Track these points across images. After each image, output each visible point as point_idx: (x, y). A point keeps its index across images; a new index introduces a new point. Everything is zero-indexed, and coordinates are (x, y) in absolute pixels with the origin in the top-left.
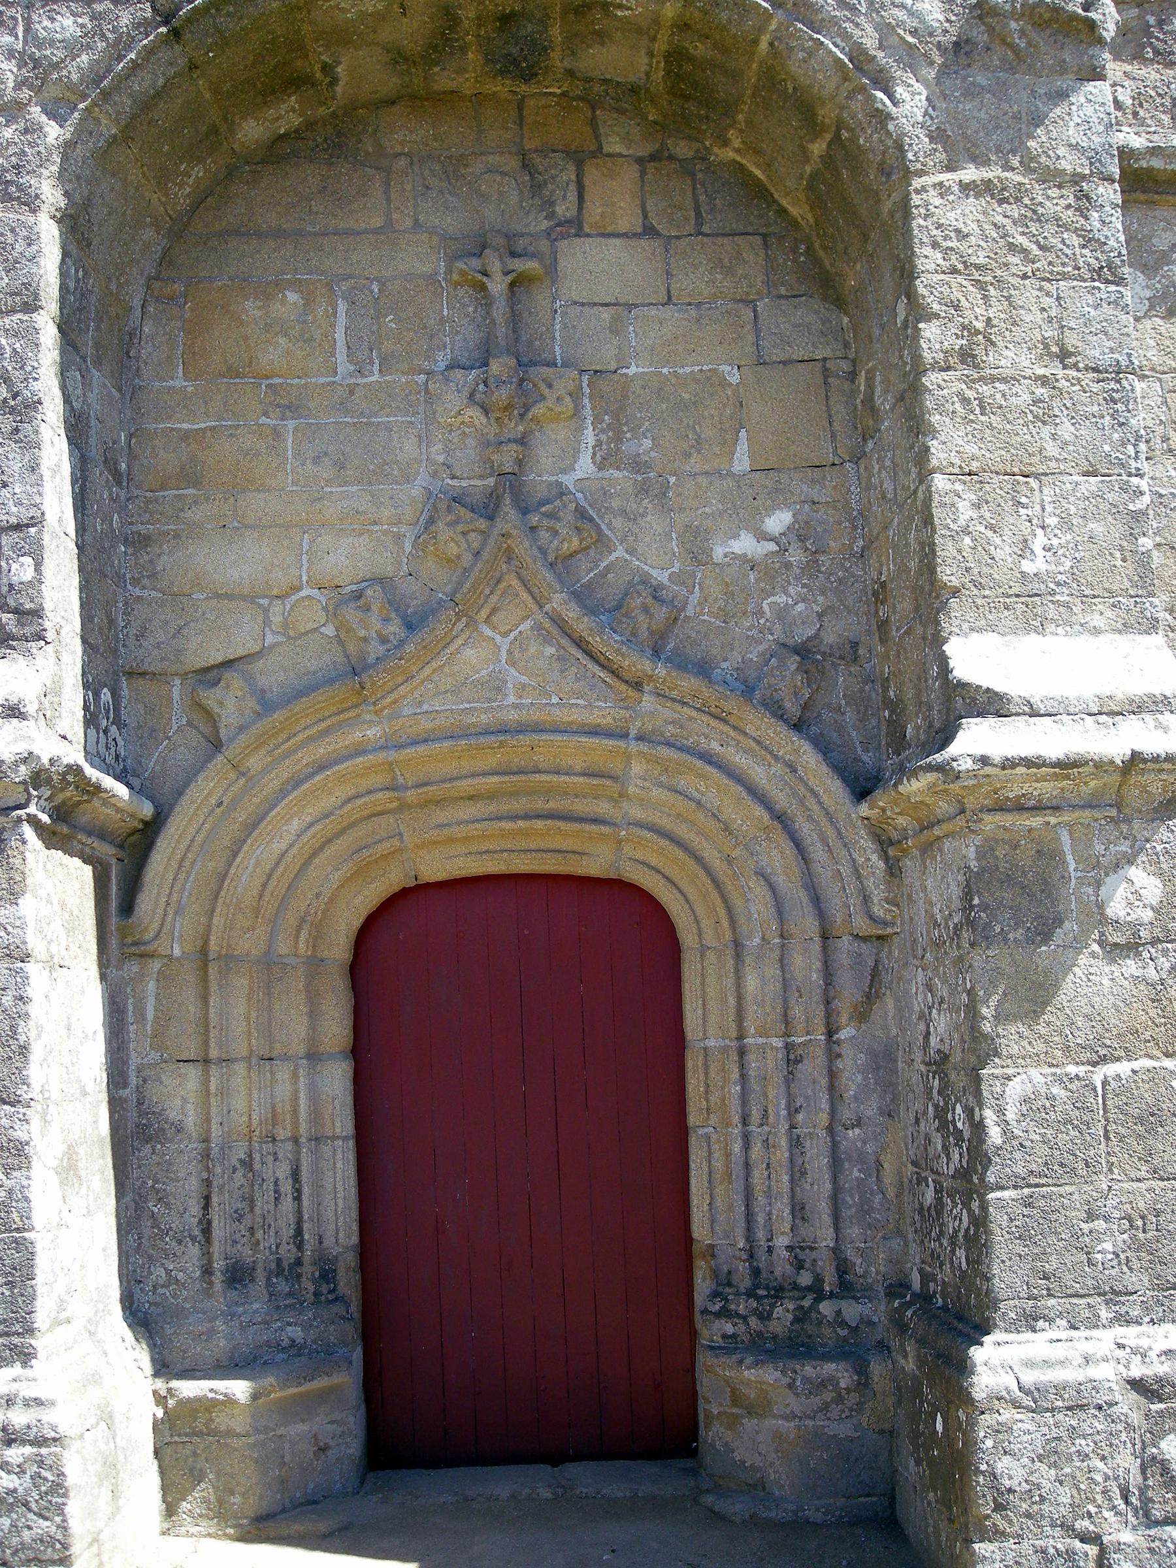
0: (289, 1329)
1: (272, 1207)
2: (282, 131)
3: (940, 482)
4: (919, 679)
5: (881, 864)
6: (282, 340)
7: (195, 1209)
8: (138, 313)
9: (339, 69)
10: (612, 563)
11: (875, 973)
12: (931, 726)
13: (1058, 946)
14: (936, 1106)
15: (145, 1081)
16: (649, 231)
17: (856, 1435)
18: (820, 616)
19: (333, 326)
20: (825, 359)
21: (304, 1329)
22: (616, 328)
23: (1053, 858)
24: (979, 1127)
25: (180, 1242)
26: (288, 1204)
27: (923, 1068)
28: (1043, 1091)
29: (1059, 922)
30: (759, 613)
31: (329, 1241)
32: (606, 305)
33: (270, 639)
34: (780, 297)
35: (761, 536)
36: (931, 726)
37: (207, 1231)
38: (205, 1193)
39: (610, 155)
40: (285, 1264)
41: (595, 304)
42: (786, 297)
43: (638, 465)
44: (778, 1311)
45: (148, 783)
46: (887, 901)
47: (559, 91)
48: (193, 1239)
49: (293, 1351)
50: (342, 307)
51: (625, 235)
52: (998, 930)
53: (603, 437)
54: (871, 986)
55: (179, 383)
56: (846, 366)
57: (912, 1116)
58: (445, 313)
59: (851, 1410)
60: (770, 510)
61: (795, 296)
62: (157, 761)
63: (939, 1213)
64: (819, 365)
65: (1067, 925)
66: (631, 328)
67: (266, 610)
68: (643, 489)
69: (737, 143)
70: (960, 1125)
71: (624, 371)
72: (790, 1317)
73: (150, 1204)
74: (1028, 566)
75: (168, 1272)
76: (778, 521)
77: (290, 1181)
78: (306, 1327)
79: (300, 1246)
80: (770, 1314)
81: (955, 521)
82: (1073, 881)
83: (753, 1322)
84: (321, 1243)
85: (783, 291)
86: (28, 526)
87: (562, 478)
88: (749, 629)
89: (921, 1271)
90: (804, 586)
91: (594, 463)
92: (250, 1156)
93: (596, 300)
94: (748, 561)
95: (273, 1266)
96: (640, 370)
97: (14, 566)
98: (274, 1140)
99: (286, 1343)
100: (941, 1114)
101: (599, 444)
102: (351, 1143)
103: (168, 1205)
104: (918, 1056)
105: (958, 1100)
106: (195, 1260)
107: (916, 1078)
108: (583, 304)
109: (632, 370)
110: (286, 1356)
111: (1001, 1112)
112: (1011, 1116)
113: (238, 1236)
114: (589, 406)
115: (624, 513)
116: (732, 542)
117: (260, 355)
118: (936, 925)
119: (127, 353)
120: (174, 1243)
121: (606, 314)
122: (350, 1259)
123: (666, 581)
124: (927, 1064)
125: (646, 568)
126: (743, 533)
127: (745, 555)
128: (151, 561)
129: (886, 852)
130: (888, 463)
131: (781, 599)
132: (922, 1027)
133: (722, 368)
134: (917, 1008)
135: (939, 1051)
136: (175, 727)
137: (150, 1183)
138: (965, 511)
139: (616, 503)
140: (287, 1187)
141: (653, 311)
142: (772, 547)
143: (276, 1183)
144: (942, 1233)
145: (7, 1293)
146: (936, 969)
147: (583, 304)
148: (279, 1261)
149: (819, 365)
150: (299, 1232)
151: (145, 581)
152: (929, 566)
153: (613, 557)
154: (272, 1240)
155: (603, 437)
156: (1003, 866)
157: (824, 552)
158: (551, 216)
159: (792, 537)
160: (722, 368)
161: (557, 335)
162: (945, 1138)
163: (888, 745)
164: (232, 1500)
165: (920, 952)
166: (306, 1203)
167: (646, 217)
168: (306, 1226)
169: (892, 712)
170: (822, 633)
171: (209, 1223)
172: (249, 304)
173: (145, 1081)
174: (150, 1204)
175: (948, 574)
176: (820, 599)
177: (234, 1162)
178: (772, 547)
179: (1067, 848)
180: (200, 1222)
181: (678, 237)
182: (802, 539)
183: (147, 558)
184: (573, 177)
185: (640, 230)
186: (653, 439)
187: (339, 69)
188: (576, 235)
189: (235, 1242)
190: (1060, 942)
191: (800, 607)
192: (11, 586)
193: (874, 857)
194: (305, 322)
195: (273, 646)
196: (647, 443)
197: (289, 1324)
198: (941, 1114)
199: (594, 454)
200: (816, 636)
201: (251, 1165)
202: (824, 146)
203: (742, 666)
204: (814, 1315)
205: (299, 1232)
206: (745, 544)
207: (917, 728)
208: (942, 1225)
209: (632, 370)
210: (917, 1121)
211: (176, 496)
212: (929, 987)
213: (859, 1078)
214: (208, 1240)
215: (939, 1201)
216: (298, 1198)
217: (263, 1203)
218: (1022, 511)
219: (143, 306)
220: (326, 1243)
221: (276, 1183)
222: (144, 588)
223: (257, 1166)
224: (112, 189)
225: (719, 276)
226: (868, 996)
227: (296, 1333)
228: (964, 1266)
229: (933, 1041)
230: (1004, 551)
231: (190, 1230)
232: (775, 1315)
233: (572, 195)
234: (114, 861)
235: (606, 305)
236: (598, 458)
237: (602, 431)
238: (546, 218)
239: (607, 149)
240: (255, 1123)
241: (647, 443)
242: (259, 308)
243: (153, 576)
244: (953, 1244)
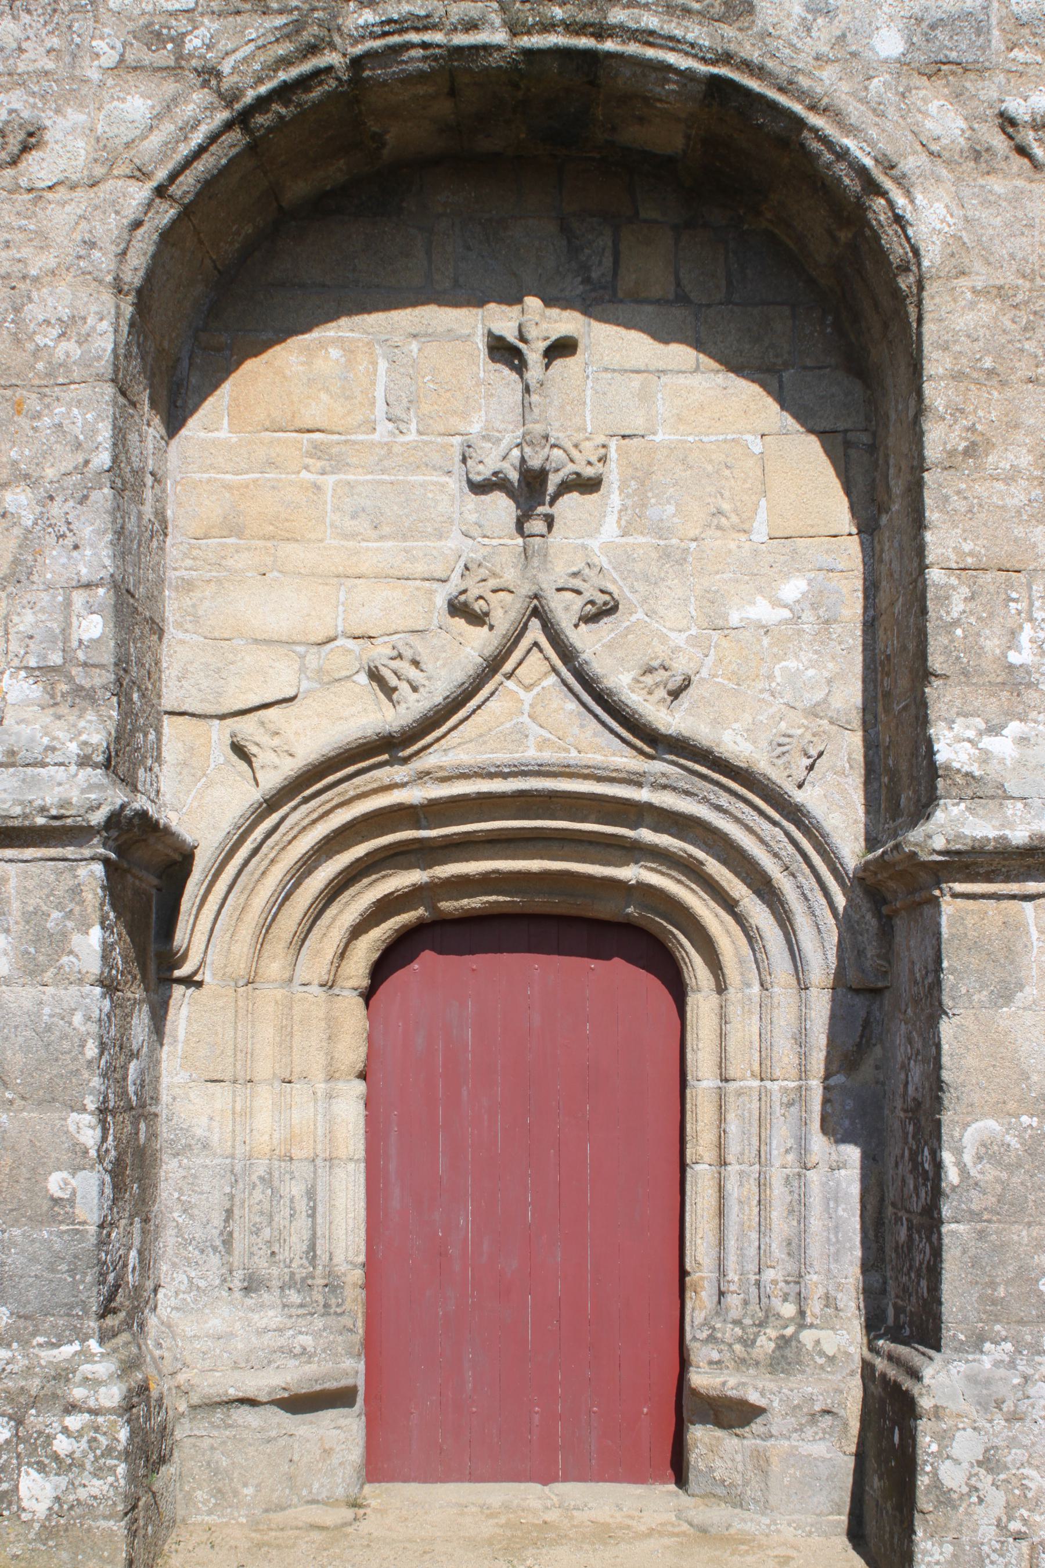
0: (301, 1337)
1: (287, 1223)
2: (328, 187)
3: (934, 575)
4: (912, 755)
5: (874, 922)
6: (324, 396)
7: (218, 1220)
8: (185, 363)
9: (387, 137)
10: (634, 624)
11: (866, 1024)
12: (919, 800)
13: (1019, 1008)
14: (910, 1149)
15: (174, 1099)
16: (682, 298)
17: (828, 1456)
18: (829, 682)
19: (373, 383)
20: (846, 431)
21: (315, 1338)
22: (645, 396)
23: (1017, 929)
24: (938, 1165)
25: (202, 1251)
26: (302, 1222)
27: (902, 1115)
28: (999, 1138)
29: (1021, 987)
30: (770, 677)
31: (339, 1258)
32: (638, 372)
33: (305, 685)
34: (805, 368)
35: (777, 603)
36: (919, 800)
37: (228, 1242)
38: (227, 1206)
39: (645, 221)
40: (298, 1277)
41: (626, 371)
42: (812, 368)
43: (660, 530)
44: (761, 1340)
45: (185, 818)
46: (878, 956)
47: (598, 156)
48: (215, 1249)
49: (304, 1359)
50: (383, 365)
51: (658, 302)
52: (964, 991)
53: (629, 503)
54: (862, 1037)
55: (223, 434)
56: (865, 438)
57: (893, 1160)
58: (482, 375)
59: (824, 1432)
60: (787, 576)
61: (820, 368)
62: (195, 797)
63: (910, 1249)
64: (840, 437)
65: (1027, 989)
66: (660, 395)
67: (302, 657)
68: (666, 554)
69: (769, 215)
70: (926, 1166)
71: (651, 437)
72: (772, 1345)
73: (176, 1215)
74: (1013, 657)
75: (190, 1280)
76: (793, 589)
77: (305, 1200)
78: (317, 1335)
79: (313, 1261)
80: (754, 1342)
81: (948, 613)
82: (1035, 950)
83: (738, 1347)
84: (331, 1259)
85: (809, 362)
86: (97, 586)
87: (588, 541)
88: (761, 691)
89: (895, 1305)
90: (816, 652)
91: (620, 527)
92: (270, 1174)
93: (627, 366)
94: (763, 627)
95: (287, 1278)
96: (667, 437)
97: (84, 623)
98: (291, 1159)
99: (298, 1350)
100: (914, 1155)
101: (624, 509)
102: (363, 1165)
103: (192, 1217)
104: (899, 1104)
105: (926, 1143)
106: (215, 1269)
107: (897, 1125)
108: (614, 371)
109: (658, 438)
110: (297, 1363)
111: (958, 1152)
112: (968, 1158)
113: (255, 1249)
114: (616, 471)
115: (646, 579)
116: (748, 608)
117: (303, 411)
118: (916, 983)
119: (175, 402)
120: (197, 1252)
121: (636, 381)
122: (357, 1275)
123: (682, 644)
124: (905, 1111)
125: (665, 631)
126: (759, 598)
127: (760, 621)
128: (194, 606)
129: (879, 912)
130: (896, 545)
131: (792, 664)
132: (903, 1076)
133: (745, 437)
134: (899, 1059)
135: (914, 1099)
136: (212, 766)
137: (176, 1195)
138: (957, 606)
139: (638, 567)
140: (302, 1205)
141: (682, 380)
142: (786, 614)
143: (292, 1200)
144: (911, 1267)
145: (70, 1279)
146: (914, 1024)
147: (614, 371)
148: (292, 1275)
149: (840, 437)
150: (312, 1247)
151: (188, 626)
152: (922, 655)
153: (633, 618)
154: (287, 1253)
155: (629, 503)
156: (971, 934)
157: (835, 621)
158: (587, 280)
159: (806, 605)
160: (745, 437)
161: (588, 401)
162: (916, 1179)
163: (886, 810)
164: (245, 1491)
165: (903, 1007)
166: (319, 1220)
167: (678, 284)
168: (319, 1242)
169: (891, 780)
170: (830, 699)
171: (231, 1234)
172: (293, 359)
173: (174, 1099)
174: (176, 1215)
175: (936, 662)
176: (830, 665)
177: (254, 1178)
178: (786, 614)
179: (1031, 921)
180: (221, 1234)
181: (709, 306)
182: (814, 607)
183: (190, 603)
184: (610, 244)
185: (671, 297)
186: (677, 504)
187: (387, 137)
188: (610, 301)
189: (252, 1254)
190: (1021, 1005)
191: (811, 672)
192: (80, 642)
193: (869, 916)
194: (346, 378)
195: (308, 691)
196: (671, 509)
197: (300, 1333)
198: (914, 1155)
199: (620, 518)
200: (825, 700)
201: (271, 1181)
202: (850, 235)
203: (752, 727)
204: (794, 1343)
205: (312, 1247)
206: (762, 611)
207: (909, 799)
208: (912, 1260)
209: (658, 438)
210: (897, 1165)
211: (220, 544)
212: (910, 1040)
213: (847, 1123)
214: (229, 1251)
215: (910, 1237)
216: (313, 1216)
217: (281, 1218)
218: (1012, 605)
219: (190, 358)
220: (335, 1261)
221: (292, 1200)
222: (186, 631)
223: (276, 1183)
224: (172, 258)
225: (747, 346)
226: (859, 1045)
227: (307, 1340)
228: (926, 1295)
229: (911, 1089)
230: (992, 644)
231: (211, 1240)
232: (758, 1343)
233: (608, 261)
234: (154, 891)
235: (638, 372)
236: (623, 523)
237: (628, 496)
238: (582, 282)
239: (643, 215)
240: (275, 1142)
241: (671, 509)
242: (303, 364)
243: (196, 620)
244: (919, 1276)
